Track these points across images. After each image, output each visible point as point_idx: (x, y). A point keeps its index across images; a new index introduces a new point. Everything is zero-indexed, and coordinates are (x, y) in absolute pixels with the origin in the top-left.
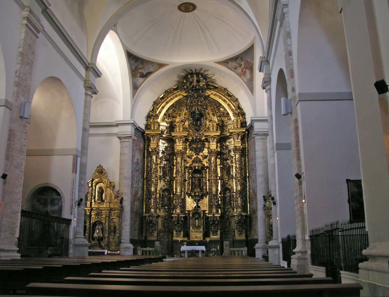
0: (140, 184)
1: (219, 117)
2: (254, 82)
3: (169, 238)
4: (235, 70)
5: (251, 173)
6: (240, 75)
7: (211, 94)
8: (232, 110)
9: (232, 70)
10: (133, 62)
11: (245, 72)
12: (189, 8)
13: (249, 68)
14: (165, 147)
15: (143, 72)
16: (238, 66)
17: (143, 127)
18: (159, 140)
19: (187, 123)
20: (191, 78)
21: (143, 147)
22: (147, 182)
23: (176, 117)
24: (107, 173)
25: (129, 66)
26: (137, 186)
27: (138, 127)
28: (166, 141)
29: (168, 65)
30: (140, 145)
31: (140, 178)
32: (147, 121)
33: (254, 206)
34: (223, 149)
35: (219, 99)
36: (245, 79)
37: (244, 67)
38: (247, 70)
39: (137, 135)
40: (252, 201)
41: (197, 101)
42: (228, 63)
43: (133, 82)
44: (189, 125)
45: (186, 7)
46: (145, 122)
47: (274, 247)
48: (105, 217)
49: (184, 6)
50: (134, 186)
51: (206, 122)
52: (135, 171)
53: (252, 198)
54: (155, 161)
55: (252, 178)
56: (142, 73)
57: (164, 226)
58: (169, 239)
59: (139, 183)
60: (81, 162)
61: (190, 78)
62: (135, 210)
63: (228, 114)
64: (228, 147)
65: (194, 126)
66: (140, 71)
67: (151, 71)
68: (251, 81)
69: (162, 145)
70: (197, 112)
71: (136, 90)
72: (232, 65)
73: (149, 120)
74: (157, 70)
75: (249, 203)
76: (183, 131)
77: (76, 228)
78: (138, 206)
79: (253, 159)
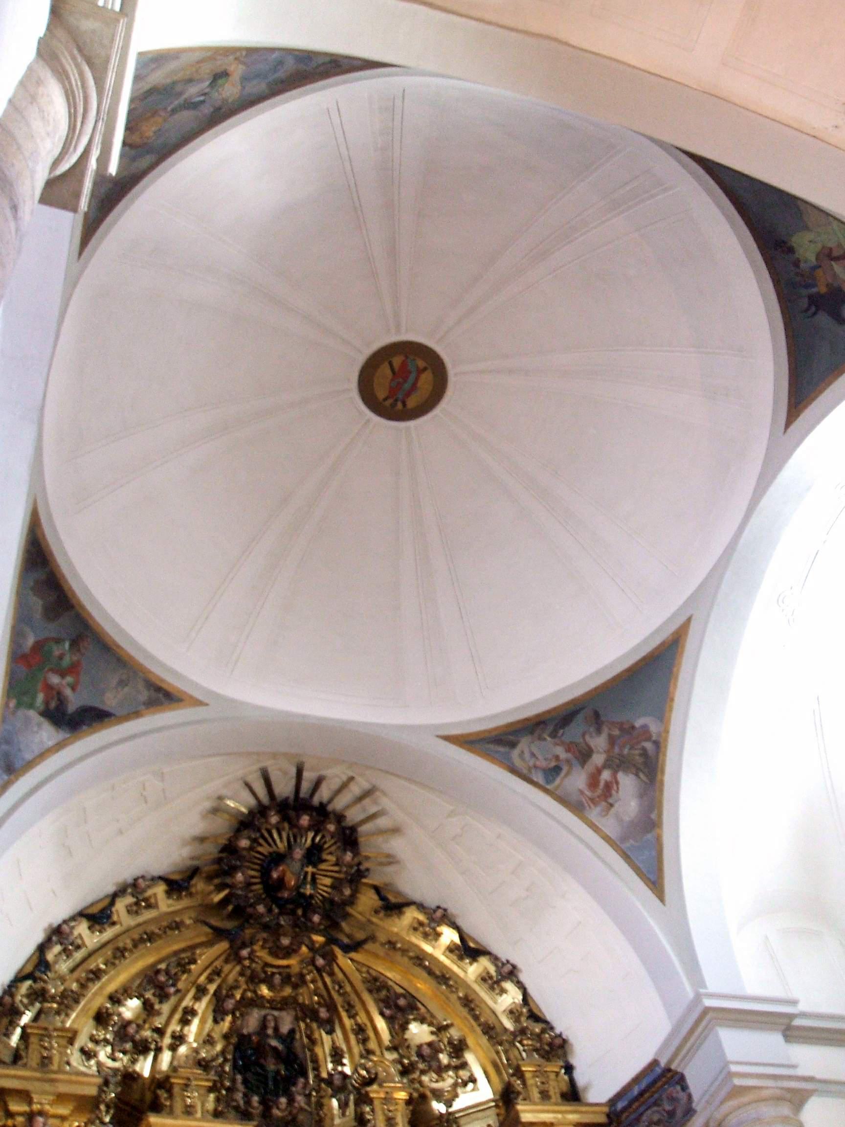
4: (548, 782)
6: (577, 808)
10: (37, 604)
11: (608, 786)
13: (639, 760)
15: (68, 692)
16: (568, 761)
25: (12, 610)
29: (198, 703)
36: (610, 825)
37: (607, 760)
38: (621, 776)
41: (280, 974)
42: (513, 745)
45: (400, 374)
66: (55, 680)
67: (106, 708)
70: (274, 1043)
71: (61, 735)
72: (533, 755)
74: (137, 714)
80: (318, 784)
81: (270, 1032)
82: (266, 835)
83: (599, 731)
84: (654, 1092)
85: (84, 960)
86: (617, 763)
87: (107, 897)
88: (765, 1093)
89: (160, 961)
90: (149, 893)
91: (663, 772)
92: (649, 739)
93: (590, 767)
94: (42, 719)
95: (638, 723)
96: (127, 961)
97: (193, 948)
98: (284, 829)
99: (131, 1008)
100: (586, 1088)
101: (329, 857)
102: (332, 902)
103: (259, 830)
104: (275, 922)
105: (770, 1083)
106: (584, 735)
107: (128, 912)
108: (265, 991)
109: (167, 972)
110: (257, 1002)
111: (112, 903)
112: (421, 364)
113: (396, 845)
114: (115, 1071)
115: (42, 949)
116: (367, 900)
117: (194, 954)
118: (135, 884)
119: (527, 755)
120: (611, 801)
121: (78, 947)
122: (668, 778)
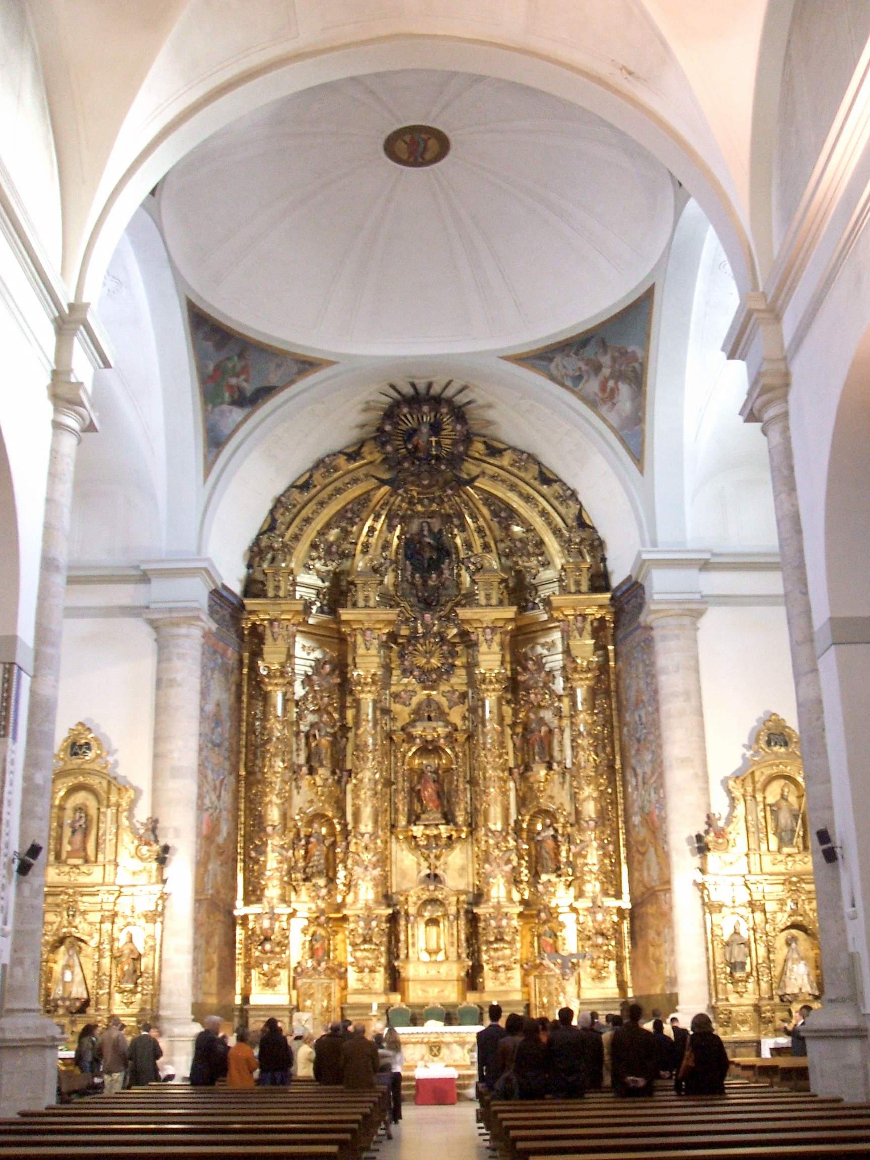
0: (227, 797)
1: (507, 556)
2: (647, 427)
3: (330, 995)
4: (576, 386)
5: (633, 752)
6: (592, 404)
7: (478, 476)
8: (556, 532)
9: (562, 385)
10: (209, 345)
12: (425, 149)
13: (631, 375)
14: (313, 663)
15: (245, 385)
16: (587, 372)
17: (237, 588)
18: (294, 636)
19: (389, 579)
20: (409, 416)
21: (236, 663)
22: (248, 787)
23: (354, 555)
24: (116, 751)
25: (193, 361)
26: (216, 803)
27: (220, 586)
28: (318, 641)
29: (331, 363)
30: (225, 651)
31: (226, 773)
32: (250, 566)
33: (649, 875)
34: (525, 669)
35: (510, 494)
36: (614, 420)
37: (611, 373)
38: (620, 385)
39: (217, 617)
40: (638, 857)
41: (427, 498)
42: (551, 360)
43: (206, 419)
44: (396, 586)
45: (413, 144)
46: (242, 572)
47: (842, 1034)
48: (98, 919)
49: (407, 138)
50: (207, 802)
51: (459, 575)
52: (210, 745)
53: (643, 843)
54: (279, 712)
55: (639, 771)
56: (240, 390)
57: (313, 953)
58: (329, 1000)
59: (223, 793)
60: (33, 693)
61: (405, 416)
62: (210, 892)
63: (541, 543)
64: (544, 661)
65: (417, 589)
66: (233, 381)
68: (636, 425)
69: (304, 655)
70: (428, 540)
71: (246, 411)
72: (564, 367)
73: (256, 564)
74: (292, 382)
75: (629, 864)
76: (378, 604)
77: (8, 969)
78: (219, 878)
79: (639, 704)
80: (430, 385)
81: (426, 533)
82: (403, 418)
83: (605, 352)
86: (619, 376)
88: (671, 613)
91: (646, 386)
92: (636, 360)
93: (600, 377)
94: (231, 407)
95: (630, 349)
105: (676, 607)
106: (596, 353)
108: (419, 508)
109: (352, 510)
110: (417, 514)
112: (424, 136)
113: (491, 414)
114: (329, 571)
116: (478, 447)
119: (560, 367)
120: (614, 401)
122: (649, 389)
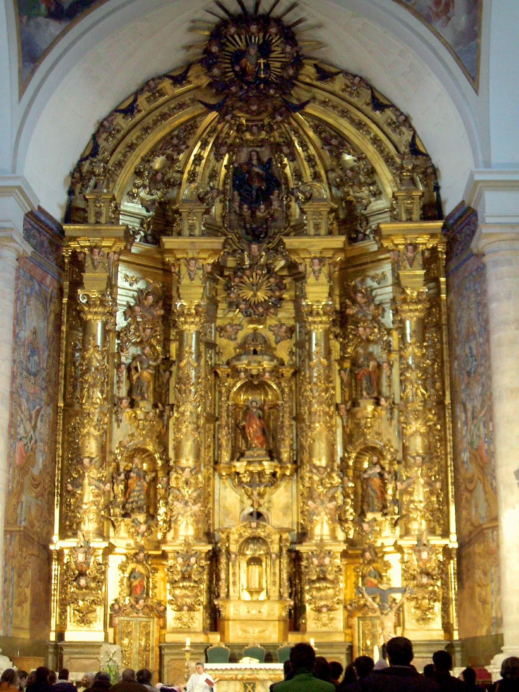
36: (448, 35)
41: (256, 125)
70: (257, 170)
71: (64, 25)
81: (255, 162)
82: (231, 39)
84: (466, 218)
85: (124, 137)
87: (132, 95)
89: (174, 130)
90: (160, 87)
94: (48, 20)
96: (150, 135)
97: (194, 118)
98: (242, 34)
99: (158, 163)
100: (445, 202)
101: (276, 49)
102: (282, 77)
103: (225, 37)
104: (245, 96)
107: (148, 102)
108: (248, 136)
110: (244, 143)
111: (135, 100)
113: (322, 35)
115: (95, 137)
116: (309, 70)
117: (195, 122)
118: (147, 83)
120: (449, 15)
121: (118, 131)
